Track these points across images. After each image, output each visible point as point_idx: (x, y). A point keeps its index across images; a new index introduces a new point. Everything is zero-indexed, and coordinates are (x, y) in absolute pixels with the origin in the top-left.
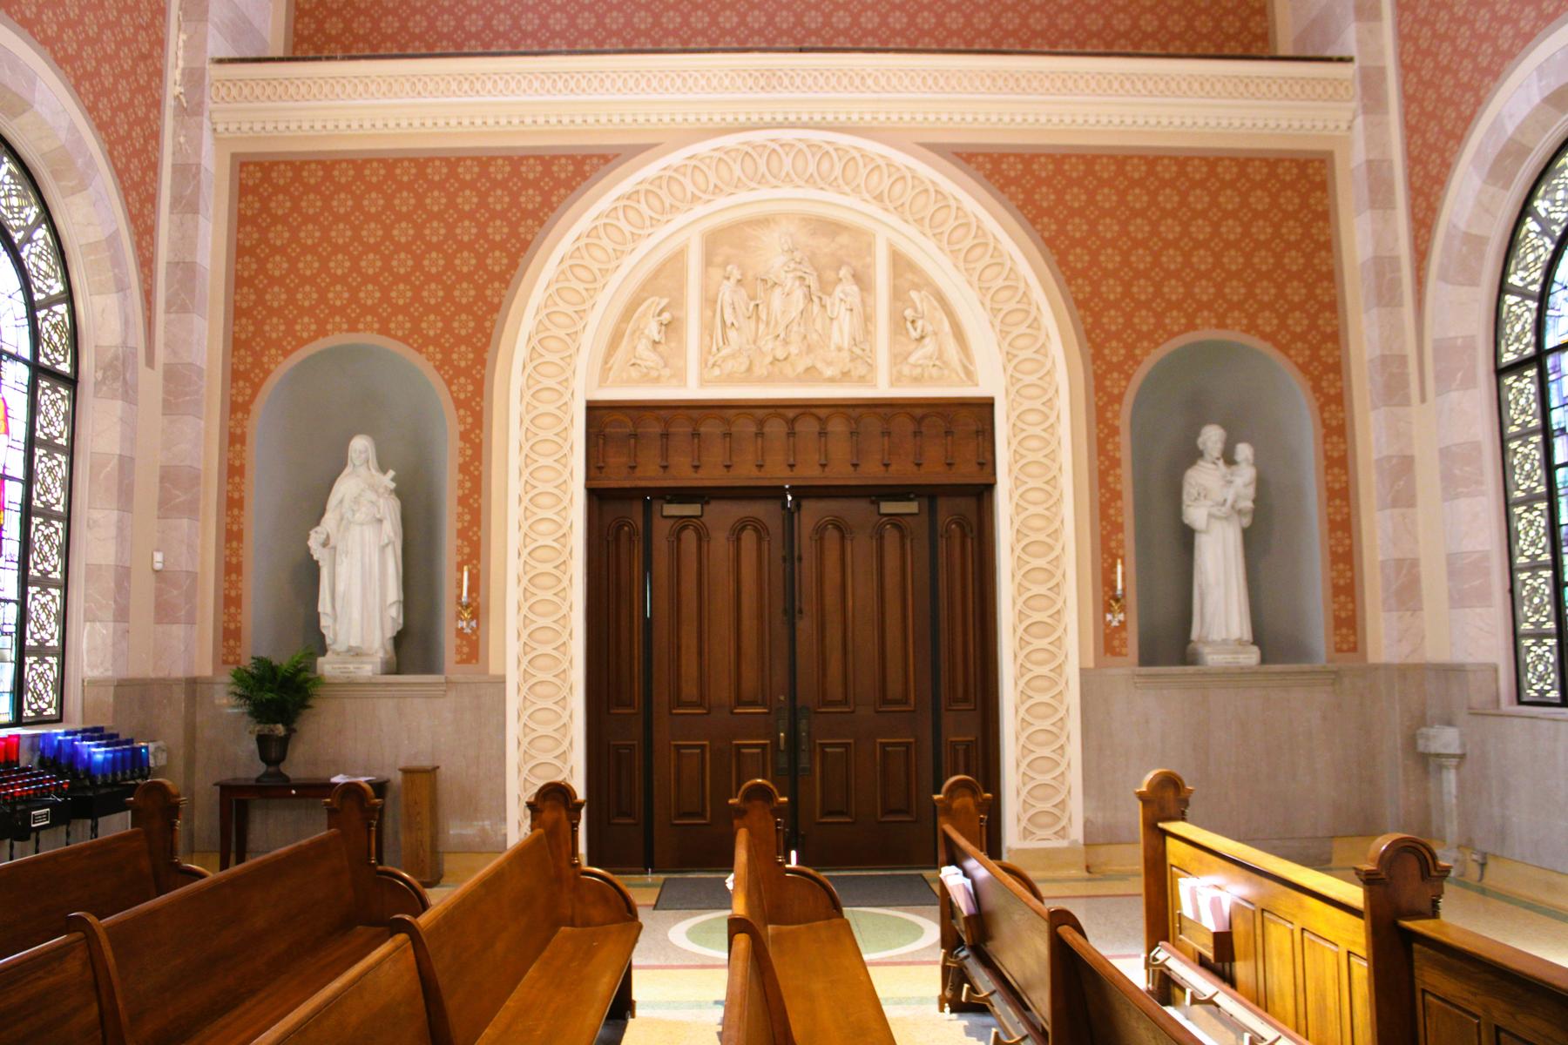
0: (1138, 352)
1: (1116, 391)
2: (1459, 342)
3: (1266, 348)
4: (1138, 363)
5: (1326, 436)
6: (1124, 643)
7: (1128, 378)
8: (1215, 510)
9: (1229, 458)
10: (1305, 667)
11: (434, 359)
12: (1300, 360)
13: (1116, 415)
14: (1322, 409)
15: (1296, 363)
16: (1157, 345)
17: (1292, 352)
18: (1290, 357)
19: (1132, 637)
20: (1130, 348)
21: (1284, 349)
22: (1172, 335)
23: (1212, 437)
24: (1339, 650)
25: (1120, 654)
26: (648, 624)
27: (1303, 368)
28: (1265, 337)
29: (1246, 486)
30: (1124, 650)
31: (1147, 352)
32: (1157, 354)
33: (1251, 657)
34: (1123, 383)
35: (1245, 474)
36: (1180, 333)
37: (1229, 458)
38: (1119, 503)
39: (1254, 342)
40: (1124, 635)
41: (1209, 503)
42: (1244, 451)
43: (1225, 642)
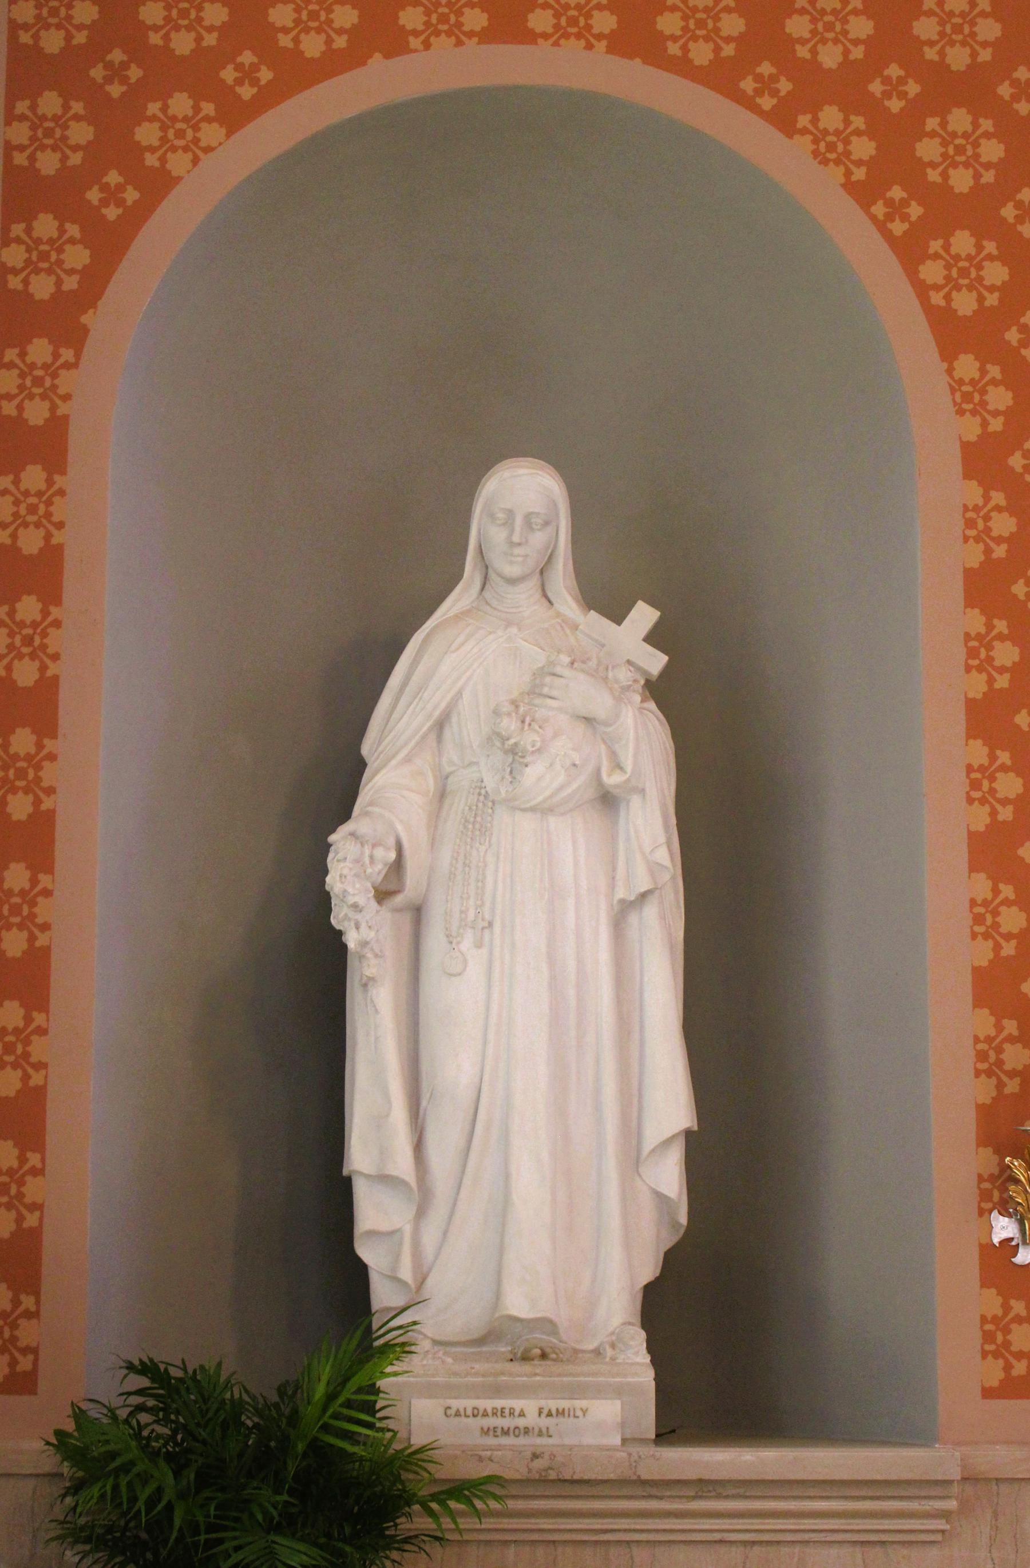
0: (831, 117)
31: (828, 151)
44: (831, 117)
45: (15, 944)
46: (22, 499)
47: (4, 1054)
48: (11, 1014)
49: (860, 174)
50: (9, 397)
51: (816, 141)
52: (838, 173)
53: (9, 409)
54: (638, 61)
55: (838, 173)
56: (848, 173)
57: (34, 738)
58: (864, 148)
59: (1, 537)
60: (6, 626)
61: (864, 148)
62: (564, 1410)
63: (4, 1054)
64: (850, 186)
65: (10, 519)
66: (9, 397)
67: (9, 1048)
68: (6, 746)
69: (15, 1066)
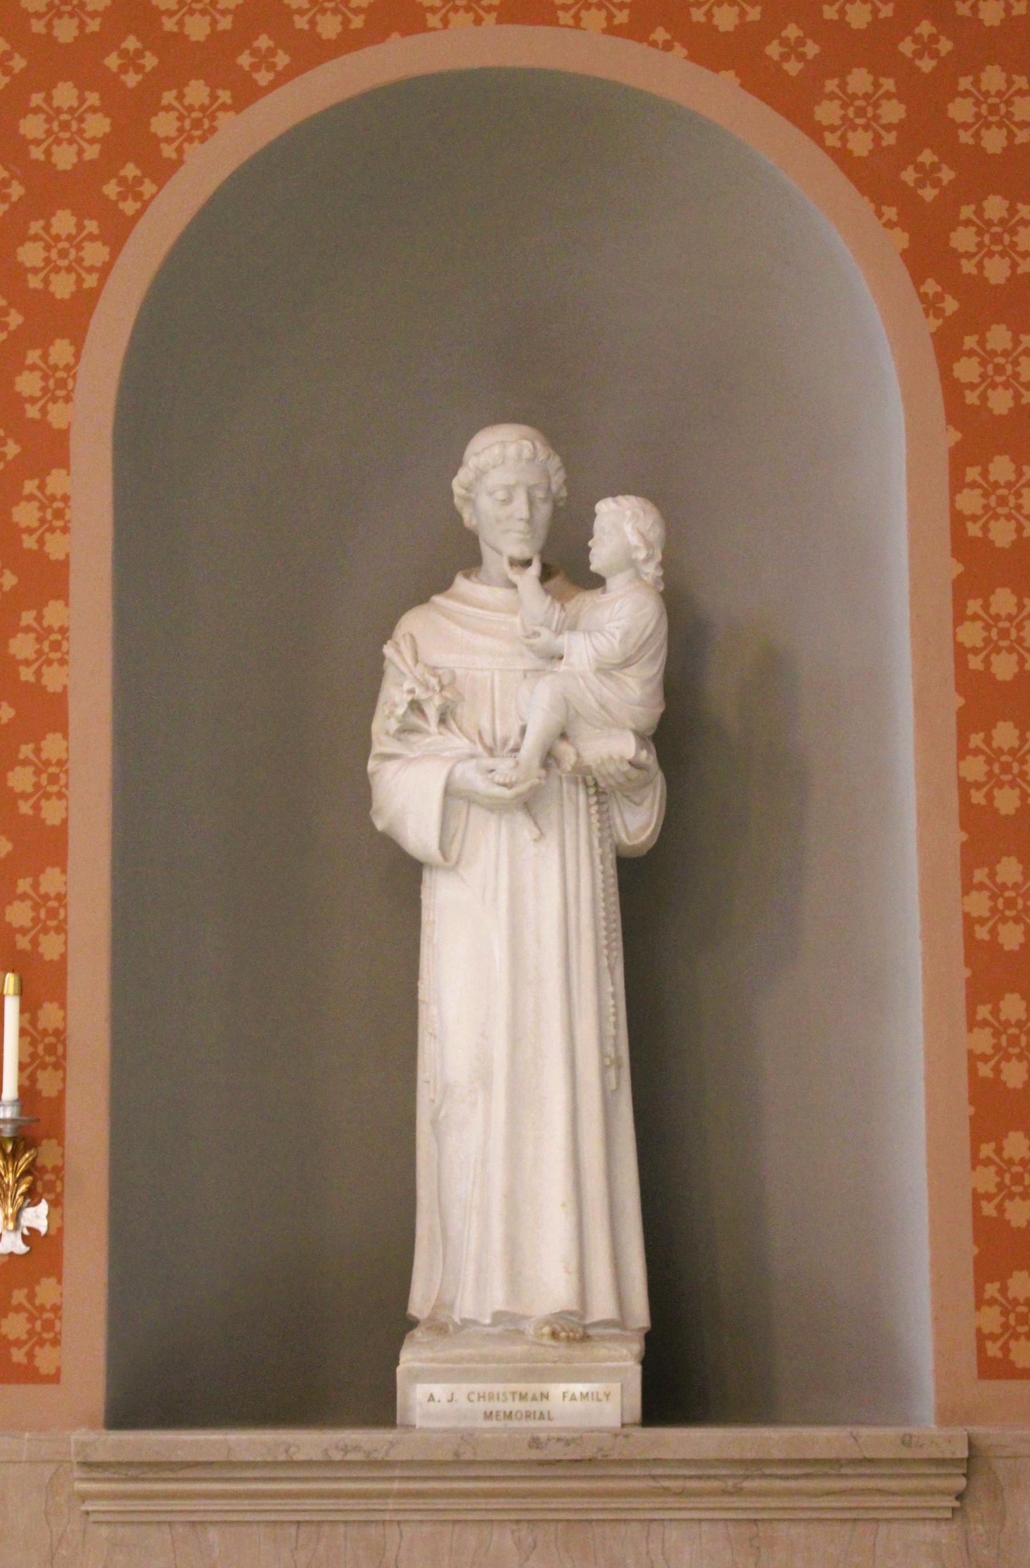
0: (163, 125)
1: (63, 287)
2: (660, 35)
3: (717, 97)
4: (162, 171)
5: (960, 459)
6: (46, 1327)
7: (117, 232)
8: (471, 776)
9: (565, 564)
10: (877, 1438)
11: (939, 313)
12: (860, 144)
13: (60, 386)
14: (947, 348)
15: (841, 157)
16: (247, 94)
17: (827, 112)
18: (815, 132)
19: (83, 1294)
20: (131, 112)
21: (794, 102)
22: (311, 52)
23: (499, 472)
24: (992, 1368)
25: (29, 1374)
26: (488, 1416)
27: (873, 179)
28: (709, 50)
29: (605, 670)
30: (45, 1360)
31: (200, 126)
32: (242, 136)
33: (598, 1396)
34: (95, 253)
35: (624, 614)
36: (350, 41)
37: (565, 564)
38: (52, 746)
39: (663, 72)
40: (47, 1291)
41: (459, 744)
42: (622, 528)
43: (508, 1324)
44: (163, 125)
45: (1016, 1145)
46: (1013, 511)
47: (1027, 1315)
48: (1019, 1213)
49: (225, 96)
50: (1021, 93)
51: (190, 139)
52: (224, 119)
53: (1021, 82)
54: (395, 36)
55: (224, 119)
56: (224, 107)
57: (1003, 1077)
58: (197, 92)
59: (1029, 340)
60: (1023, 385)
61: (197, 92)
62: (526, 1394)
63: (1027, 1315)
64: (239, 105)
65: (1022, 359)
66: (1021, 93)
67: (1022, 1319)
68: (1024, 796)
69: (1015, 1302)
